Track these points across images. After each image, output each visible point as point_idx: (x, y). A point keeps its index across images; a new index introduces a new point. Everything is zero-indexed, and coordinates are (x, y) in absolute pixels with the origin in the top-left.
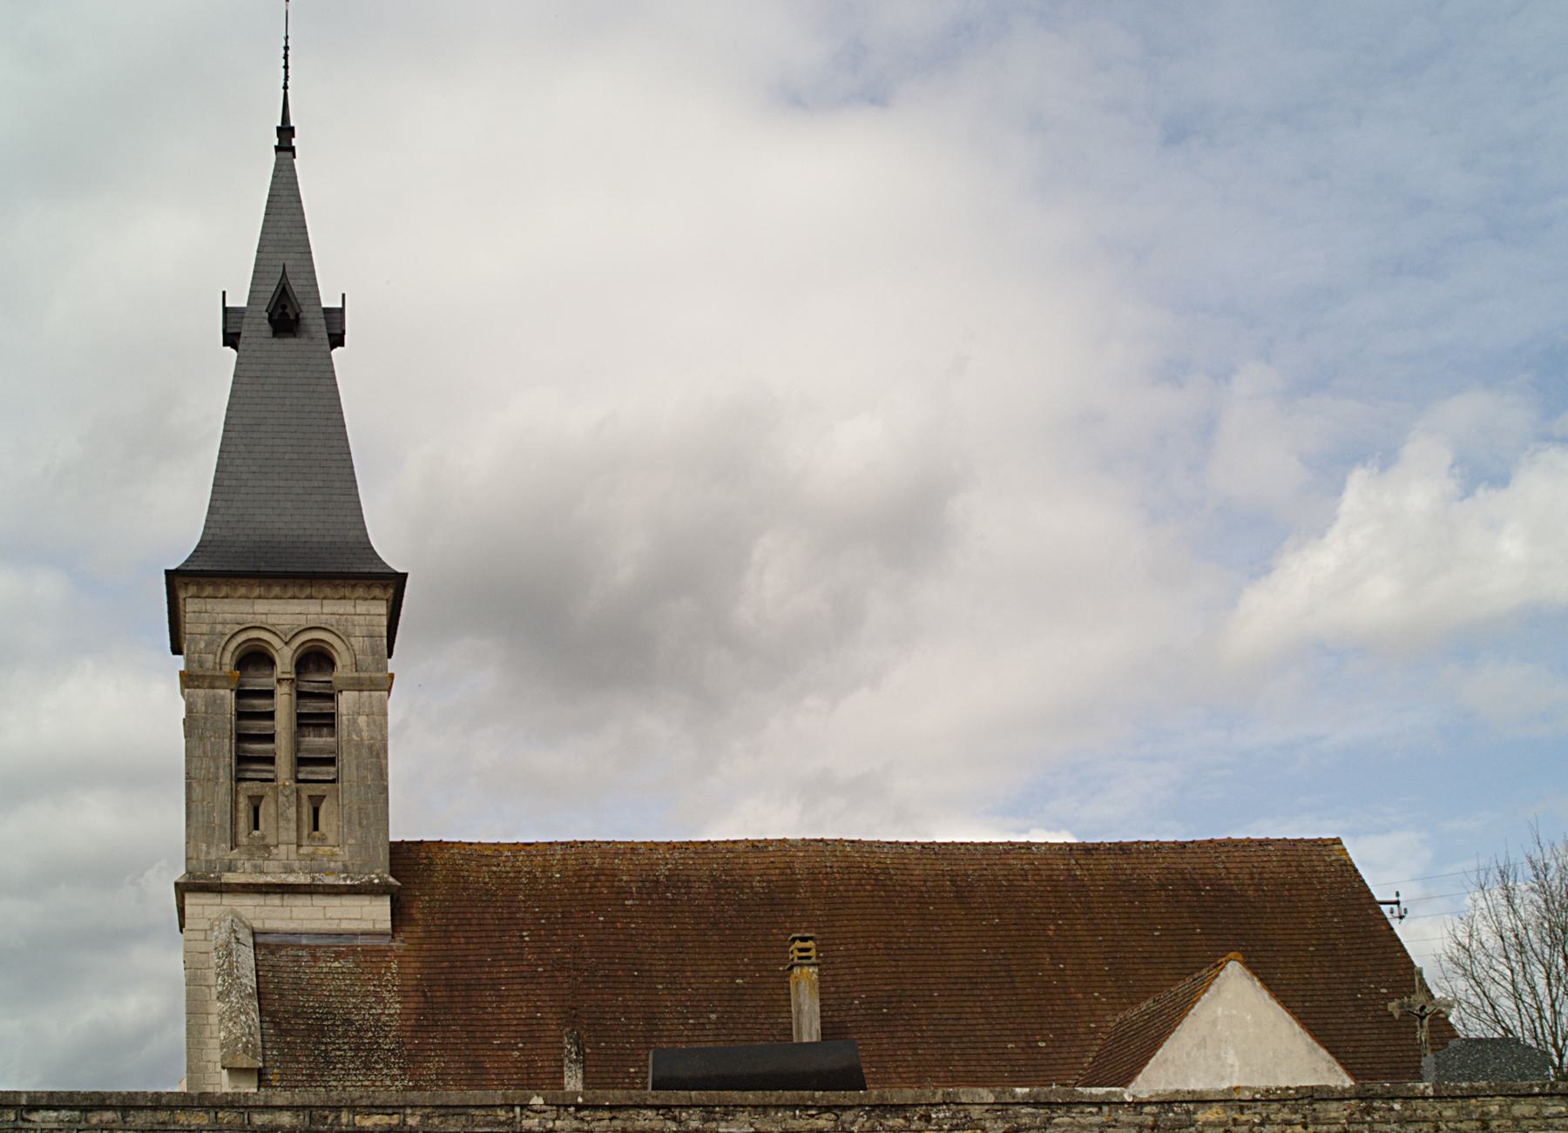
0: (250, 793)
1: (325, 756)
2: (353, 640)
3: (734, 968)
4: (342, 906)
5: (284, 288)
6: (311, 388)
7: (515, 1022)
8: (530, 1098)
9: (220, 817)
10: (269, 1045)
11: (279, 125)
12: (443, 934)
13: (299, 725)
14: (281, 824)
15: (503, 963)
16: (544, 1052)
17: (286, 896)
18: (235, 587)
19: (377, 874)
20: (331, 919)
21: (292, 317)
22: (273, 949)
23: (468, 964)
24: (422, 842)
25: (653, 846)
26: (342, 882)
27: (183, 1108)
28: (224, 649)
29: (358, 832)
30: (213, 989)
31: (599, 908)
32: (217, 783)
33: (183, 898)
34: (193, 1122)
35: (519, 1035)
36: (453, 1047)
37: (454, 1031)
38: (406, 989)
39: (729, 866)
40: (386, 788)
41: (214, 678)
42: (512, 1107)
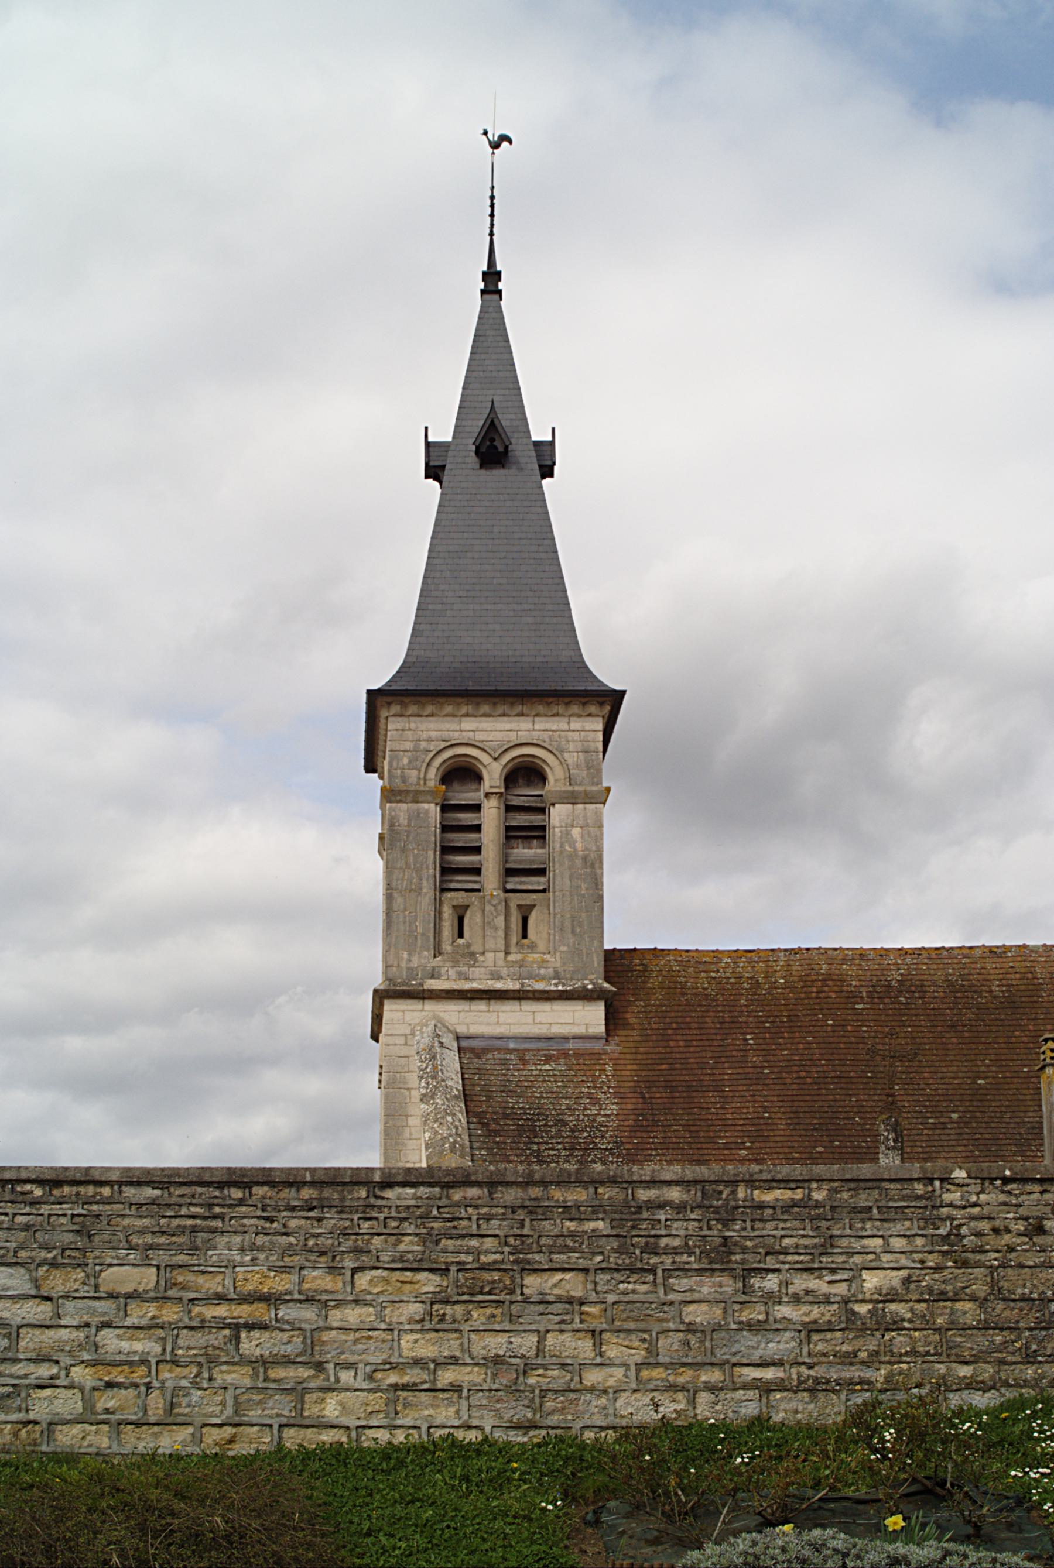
0: (455, 903)
1: (535, 867)
2: (566, 755)
3: (974, 1069)
4: (552, 1011)
5: (492, 422)
6: (521, 516)
7: (742, 1122)
8: (952, 1171)
9: (423, 925)
10: (477, 1145)
11: (485, 269)
12: (660, 1038)
13: (508, 838)
14: (488, 933)
15: (726, 1065)
16: (774, 1150)
17: (492, 1002)
18: (423, 705)
19: (591, 980)
20: (541, 1023)
21: (501, 449)
22: (479, 1053)
23: (689, 1066)
24: (635, 950)
25: (883, 953)
26: (553, 988)
27: (558, 1184)
28: (429, 765)
29: (571, 939)
30: (413, 1093)
31: (828, 1012)
32: (420, 894)
33: (382, 1004)
34: (570, 1198)
35: (746, 1134)
36: (676, 1146)
37: (675, 1131)
38: (622, 1090)
39: (966, 971)
40: (601, 898)
41: (417, 792)
42: (931, 1180)
